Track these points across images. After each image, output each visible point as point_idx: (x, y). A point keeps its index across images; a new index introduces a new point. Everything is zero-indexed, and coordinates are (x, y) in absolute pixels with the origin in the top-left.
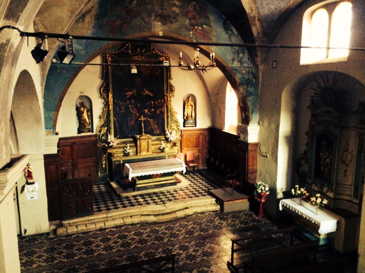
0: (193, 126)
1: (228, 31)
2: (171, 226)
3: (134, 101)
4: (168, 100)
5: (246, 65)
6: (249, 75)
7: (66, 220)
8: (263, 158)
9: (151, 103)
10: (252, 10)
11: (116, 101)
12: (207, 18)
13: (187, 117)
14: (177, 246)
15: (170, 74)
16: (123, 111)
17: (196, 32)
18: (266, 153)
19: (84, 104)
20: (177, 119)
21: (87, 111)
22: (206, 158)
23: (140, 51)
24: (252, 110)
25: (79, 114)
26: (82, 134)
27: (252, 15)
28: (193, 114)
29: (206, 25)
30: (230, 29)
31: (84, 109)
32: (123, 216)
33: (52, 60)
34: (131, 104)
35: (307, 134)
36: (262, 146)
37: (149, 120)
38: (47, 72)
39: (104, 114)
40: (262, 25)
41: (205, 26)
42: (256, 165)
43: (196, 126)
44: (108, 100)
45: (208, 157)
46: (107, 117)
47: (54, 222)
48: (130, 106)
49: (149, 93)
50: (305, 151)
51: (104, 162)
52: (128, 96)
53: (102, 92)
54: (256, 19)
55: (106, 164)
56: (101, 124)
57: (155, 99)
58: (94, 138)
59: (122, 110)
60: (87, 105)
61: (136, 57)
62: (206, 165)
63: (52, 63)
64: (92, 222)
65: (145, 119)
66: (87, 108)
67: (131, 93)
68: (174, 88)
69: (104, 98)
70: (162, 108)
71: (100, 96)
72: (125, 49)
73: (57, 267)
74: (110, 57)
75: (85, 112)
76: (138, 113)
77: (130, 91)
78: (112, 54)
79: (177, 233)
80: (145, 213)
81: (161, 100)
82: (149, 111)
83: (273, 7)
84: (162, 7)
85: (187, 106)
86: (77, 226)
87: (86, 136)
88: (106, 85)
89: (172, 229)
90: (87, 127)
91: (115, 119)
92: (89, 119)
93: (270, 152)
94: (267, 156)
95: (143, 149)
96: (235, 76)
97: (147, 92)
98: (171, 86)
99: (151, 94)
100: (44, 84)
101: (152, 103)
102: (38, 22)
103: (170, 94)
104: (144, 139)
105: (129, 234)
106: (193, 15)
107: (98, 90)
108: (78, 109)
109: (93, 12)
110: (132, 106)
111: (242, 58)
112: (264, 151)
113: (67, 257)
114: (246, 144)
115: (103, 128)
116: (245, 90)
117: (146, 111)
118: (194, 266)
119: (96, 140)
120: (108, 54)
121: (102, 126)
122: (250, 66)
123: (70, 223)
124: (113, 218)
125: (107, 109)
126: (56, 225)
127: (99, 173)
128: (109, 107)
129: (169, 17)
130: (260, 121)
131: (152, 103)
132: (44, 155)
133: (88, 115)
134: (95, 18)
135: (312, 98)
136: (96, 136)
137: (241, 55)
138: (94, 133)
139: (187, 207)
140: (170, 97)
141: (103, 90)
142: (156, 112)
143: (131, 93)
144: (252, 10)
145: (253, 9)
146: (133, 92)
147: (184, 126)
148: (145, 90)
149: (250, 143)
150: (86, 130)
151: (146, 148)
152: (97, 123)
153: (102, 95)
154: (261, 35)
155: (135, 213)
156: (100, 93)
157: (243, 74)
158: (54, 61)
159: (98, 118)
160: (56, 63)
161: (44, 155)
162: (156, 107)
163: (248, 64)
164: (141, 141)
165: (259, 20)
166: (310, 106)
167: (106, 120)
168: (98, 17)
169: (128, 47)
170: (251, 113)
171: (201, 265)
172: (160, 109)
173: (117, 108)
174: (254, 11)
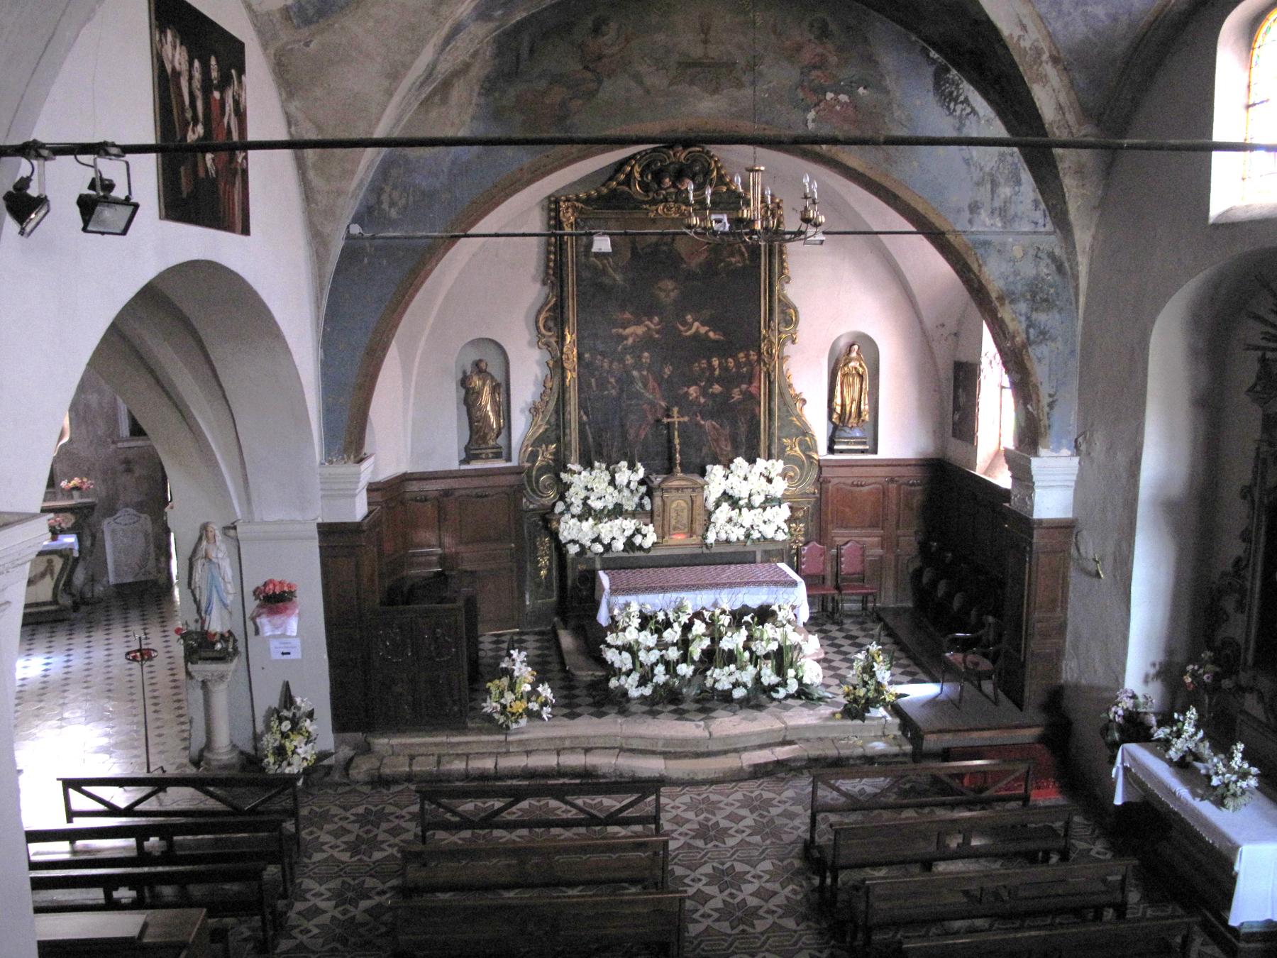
0: (863, 452)
1: (952, 105)
2: (714, 798)
3: (651, 357)
4: (771, 355)
5: (1027, 228)
6: (1037, 266)
7: (383, 735)
8: (1087, 578)
9: (710, 363)
10: (1024, 27)
11: (587, 355)
12: (870, 60)
13: (842, 416)
14: (707, 869)
15: (782, 261)
16: (613, 392)
17: (831, 111)
18: (1094, 560)
19: (483, 365)
20: (804, 424)
21: (495, 389)
22: (911, 570)
23: (674, 185)
24: (1050, 396)
25: (470, 399)
26: (476, 465)
27: (1026, 44)
28: (865, 407)
29: (865, 88)
30: (962, 98)
31: (484, 384)
32: (558, 744)
33: (348, 227)
34: (638, 365)
35: (1246, 493)
36: (1084, 533)
37: (702, 422)
38: (331, 267)
39: (546, 398)
40: (1072, 82)
41: (861, 90)
42: (1064, 609)
43: (875, 451)
44: (562, 353)
45: (917, 564)
46: (557, 411)
47: (348, 736)
48: (635, 373)
49: (703, 330)
50: (1238, 560)
51: (544, 561)
52: (630, 341)
53: (541, 325)
54: (1045, 57)
55: (550, 570)
56: (534, 433)
57: (725, 349)
58: (512, 479)
59: (609, 386)
60: (495, 369)
61: (661, 207)
62: (909, 593)
63: (349, 237)
64: (460, 752)
65: (686, 419)
66: (493, 378)
67: (640, 330)
68: (796, 311)
69: (548, 345)
70: (750, 383)
71: (536, 339)
72: (619, 184)
73: (315, 873)
74: (570, 210)
75: (487, 390)
76: (664, 400)
77: (639, 323)
78: (578, 199)
79: (724, 823)
80: (635, 744)
81: (747, 356)
82: (704, 392)
83: (1100, 11)
84: (706, 34)
85: (845, 375)
86: (412, 758)
87: (491, 469)
88: (555, 304)
89: (712, 807)
90: (491, 443)
91: (585, 418)
92: (497, 415)
93: (1109, 561)
94: (1098, 575)
95: (673, 522)
96: (980, 266)
97: (696, 324)
98: (787, 305)
99: (711, 334)
100: (325, 303)
101: (715, 362)
102: (299, 116)
103: (780, 332)
104: (677, 489)
105: (736, 827)
106: (817, 55)
107: (533, 314)
108: (464, 382)
109: (478, 71)
110: (645, 373)
111: (1007, 202)
112: (1090, 556)
113: (354, 848)
114: (1025, 523)
115: (544, 446)
116: (1023, 319)
117: (693, 391)
118: (736, 944)
119: (518, 486)
120: (564, 202)
121: (541, 440)
122: (1042, 229)
123: (392, 746)
124: (529, 748)
125: (557, 381)
126: (356, 747)
127: (527, 596)
128: (563, 378)
129: (731, 66)
130: (1080, 440)
131: (715, 362)
132: (320, 526)
133: (495, 403)
134: (482, 87)
135: (1264, 355)
136: (517, 471)
137: (1005, 191)
138: (514, 463)
139: (788, 738)
140: (782, 345)
141: (547, 319)
142: (727, 395)
143: (640, 330)
144: (1024, 27)
145: (1025, 21)
146: (647, 326)
147: (831, 450)
148: (689, 318)
149: (1040, 521)
150: (489, 451)
151: (685, 520)
152: (520, 426)
153: (544, 336)
154: (1071, 117)
155: (602, 740)
156: (538, 328)
157: (1013, 260)
158: (356, 229)
159: (527, 413)
160: (361, 236)
161: (320, 526)
162: (728, 380)
163: (1036, 223)
164: (666, 495)
165: (1055, 60)
166: (1255, 385)
167: (553, 420)
168: (490, 86)
169: (630, 175)
170: (1046, 409)
171: (762, 946)
172: (744, 387)
173: (593, 380)
174: (1030, 26)
